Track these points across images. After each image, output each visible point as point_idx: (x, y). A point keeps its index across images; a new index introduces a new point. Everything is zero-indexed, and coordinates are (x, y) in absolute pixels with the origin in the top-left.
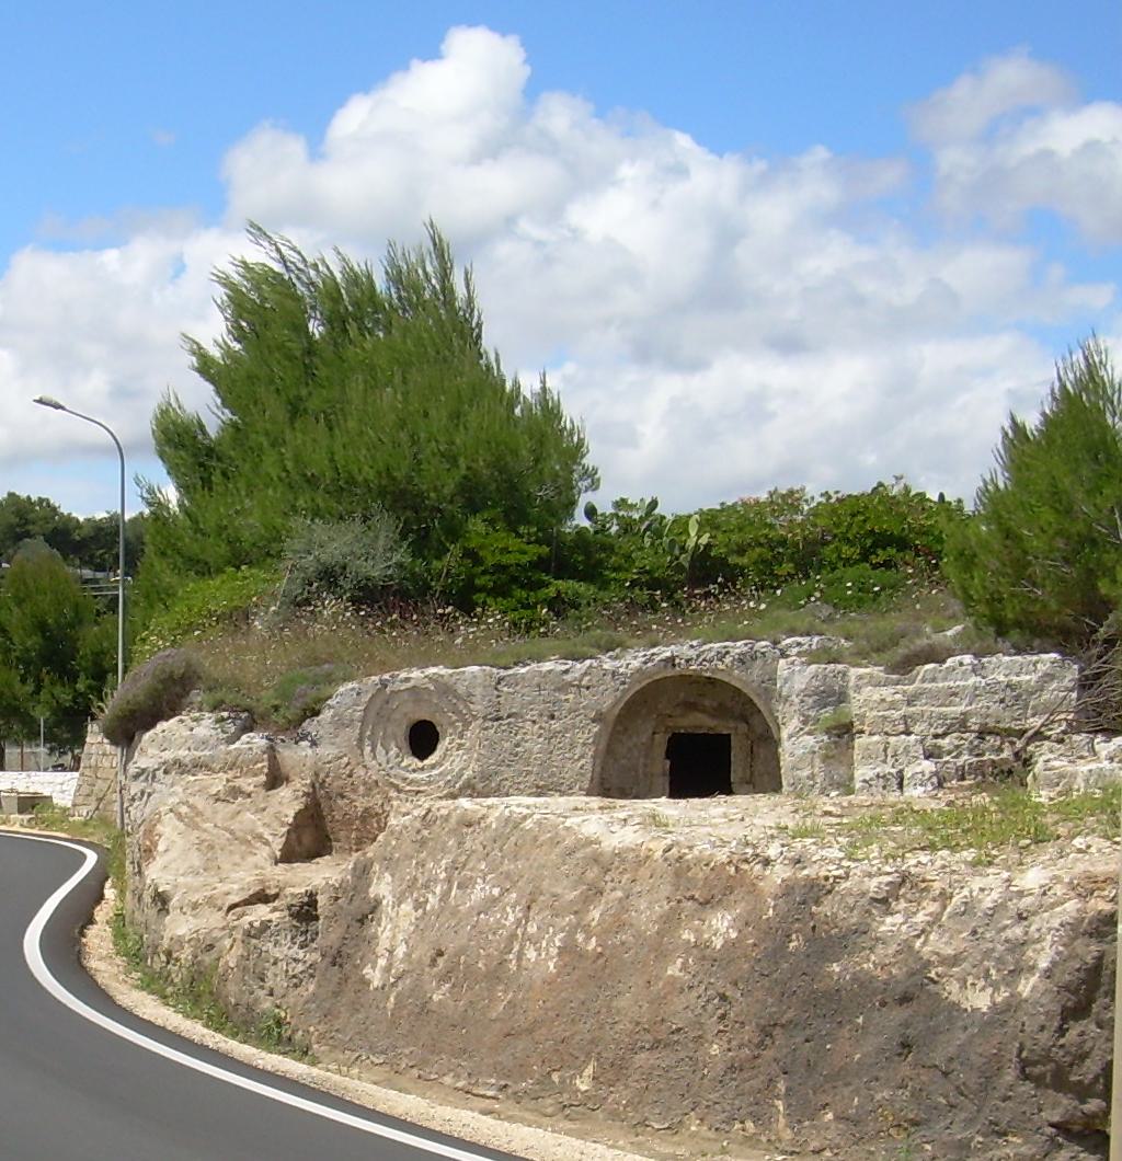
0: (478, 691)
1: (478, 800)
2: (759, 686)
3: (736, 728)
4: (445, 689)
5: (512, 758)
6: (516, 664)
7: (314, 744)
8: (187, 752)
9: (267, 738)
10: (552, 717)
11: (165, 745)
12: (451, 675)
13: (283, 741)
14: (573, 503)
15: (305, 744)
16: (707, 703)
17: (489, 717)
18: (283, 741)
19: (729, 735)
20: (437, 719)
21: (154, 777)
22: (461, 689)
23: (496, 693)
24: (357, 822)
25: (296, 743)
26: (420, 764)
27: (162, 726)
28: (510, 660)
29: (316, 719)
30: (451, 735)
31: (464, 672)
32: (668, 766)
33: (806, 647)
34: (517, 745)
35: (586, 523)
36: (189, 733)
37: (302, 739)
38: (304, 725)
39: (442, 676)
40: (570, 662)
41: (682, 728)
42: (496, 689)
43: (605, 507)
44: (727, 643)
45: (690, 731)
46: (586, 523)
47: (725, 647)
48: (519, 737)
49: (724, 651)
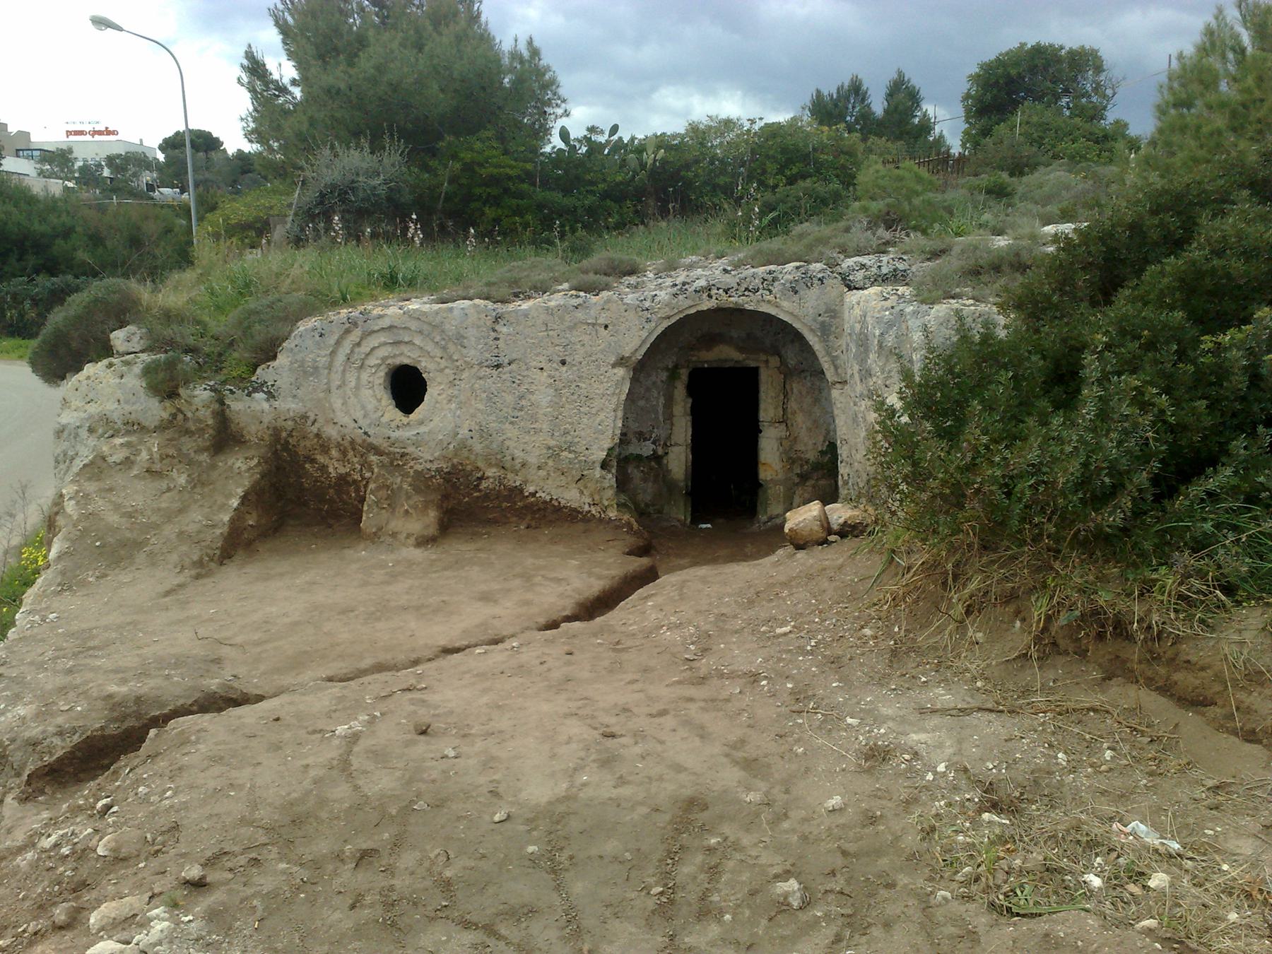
0: (472, 333)
1: (446, 710)
2: (815, 320)
3: (767, 362)
4: (431, 326)
5: (516, 413)
6: (516, 295)
7: (271, 396)
8: (116, 405)
9: (213, 389)
10: (563, 363)
11: (91, 396)
12: (437, 313)
13: (232, 392)
14: (547, 131)
15: (260, 396)
16: (734, 334)
17: (485, 364)
18: (232, 392)
19: (756, 370)
20: (424, 365)
21: (77, 435)
22: (450, 328)
23: (493, 335)
24: (331, 491)
25: (249, 395)
26: (405, 420)
27: (89, 369)
28: (504, 291)
29: (272, 364)
30: (440, 383)
31: (451, 309)
32: (689, 405)
33: (874, 270)
34: (521, 398)
35: (561, 145)
36: (118, 380)
37: (256, 390)
38: (259, 371)
39: (425, 313)
40: (582, 294)
41: (706, 362)
42: (494, 330)
43: (577, 132)
44: (772, 267)
45: (715, 365)
46: (561, 145)
47: (770, 273)
48: (522, 389)
49: (770, 277)
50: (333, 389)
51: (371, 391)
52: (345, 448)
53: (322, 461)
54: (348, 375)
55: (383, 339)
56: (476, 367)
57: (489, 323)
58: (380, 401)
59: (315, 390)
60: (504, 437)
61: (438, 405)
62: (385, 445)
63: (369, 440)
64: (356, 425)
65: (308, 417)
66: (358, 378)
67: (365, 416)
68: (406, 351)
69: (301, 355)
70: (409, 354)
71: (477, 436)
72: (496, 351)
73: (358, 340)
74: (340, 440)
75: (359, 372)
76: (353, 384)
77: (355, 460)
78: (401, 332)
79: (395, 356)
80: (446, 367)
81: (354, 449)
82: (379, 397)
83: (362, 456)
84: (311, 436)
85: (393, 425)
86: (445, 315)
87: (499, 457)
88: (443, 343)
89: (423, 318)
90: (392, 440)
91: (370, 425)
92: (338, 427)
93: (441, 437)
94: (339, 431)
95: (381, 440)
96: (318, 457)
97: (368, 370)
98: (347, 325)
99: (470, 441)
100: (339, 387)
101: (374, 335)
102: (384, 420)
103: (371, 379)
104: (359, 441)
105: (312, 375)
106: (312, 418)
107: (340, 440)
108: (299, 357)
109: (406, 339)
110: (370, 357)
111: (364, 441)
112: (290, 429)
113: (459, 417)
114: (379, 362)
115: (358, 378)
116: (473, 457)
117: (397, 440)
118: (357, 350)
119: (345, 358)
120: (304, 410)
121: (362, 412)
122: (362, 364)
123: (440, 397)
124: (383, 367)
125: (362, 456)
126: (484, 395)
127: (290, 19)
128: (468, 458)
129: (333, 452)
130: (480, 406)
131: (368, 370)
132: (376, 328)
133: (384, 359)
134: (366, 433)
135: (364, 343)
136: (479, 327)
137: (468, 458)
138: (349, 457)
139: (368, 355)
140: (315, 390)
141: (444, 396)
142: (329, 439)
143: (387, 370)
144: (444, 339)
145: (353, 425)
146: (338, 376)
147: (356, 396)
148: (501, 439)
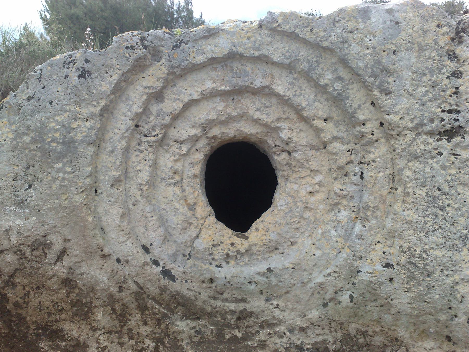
23: (451, 65)
42: (453, 56)
50: (104, 186)
51: (178, 190)
52: (125, 307)
53: (75, 333)
54: (134, 158)
55: (209, 85)
56: (410, 135)
57: (443, 41)
58: (192, 208)
59: (65, 189)
60: (457, 277)
61: (307, 214)
62: (204, 296)
63: (176, 286)
64: (147, 258)
65: (49, 246)
66: (155, 165)
67: (166, 239)
68: (251, 112)
69: (39, 116)
70: (257, 115)
71: (400, 278)
72: (452, 100)
73: (159, 85)
74: (114, 290)
75: (155, 153)
76: (144, 176)
77: (144, 330)
78: (248, 67)
79: (230, 119)
80: (335, 138)
81: (142, 308)
82: (191, 201)
83: (159, 322)
84: (54, 284)
85: (218, 254)
86: (351, 25)
87: (443, 317)
88: (338, 86)
89: (306, 34)
90: (219, 283)
91: (174, 257)
92: (111, 264)
93: (320, 279)
94: (113, 273)
95: (195, 286)
96: (67, 326)
97: (175, 148)
98: (140, 52)
99: (387, 288)
100: (116, 182)
101: (192, 77)
102: (201, 244)
103: (179, 166)
104: (153, 290)
105: (60, 157)
106: (57, 247)
107: (114, 290)
108: (32, 122)
109: (259, 83)
110: (180, 123)
111: (164, 290)
112: (8, 270)
113: (360, 237)
114: (194, 132)
115: (155, 165)
116: (388, 319)
117: (228, 284)
118: (154, 108)
119: (130, 123)
120: (41, 231)
121: (161, 231)
122: (165, 136)
123: (312, 199)
124: (202, 143)
125: (159, 322)
126: (422, 192)
127: (48, 16)
128: (378, 321)
129: (99, 316)
130: (413, 216)
131: (175, 148)
132: (200, 59)
133: (210, 124)
134: (166, 273)
135: (169, 94)
136: (421, 49)
137: (378, 321)
138: (132, 324)
139: (176, 117)
140: (65, 189)
141: (321, 196)
142: (92, 289)
143: (207, 150)
144: (340, 79)
145: (143, 258)
146: (118, 159)
147: (148, 199)
148: (449, 281)
